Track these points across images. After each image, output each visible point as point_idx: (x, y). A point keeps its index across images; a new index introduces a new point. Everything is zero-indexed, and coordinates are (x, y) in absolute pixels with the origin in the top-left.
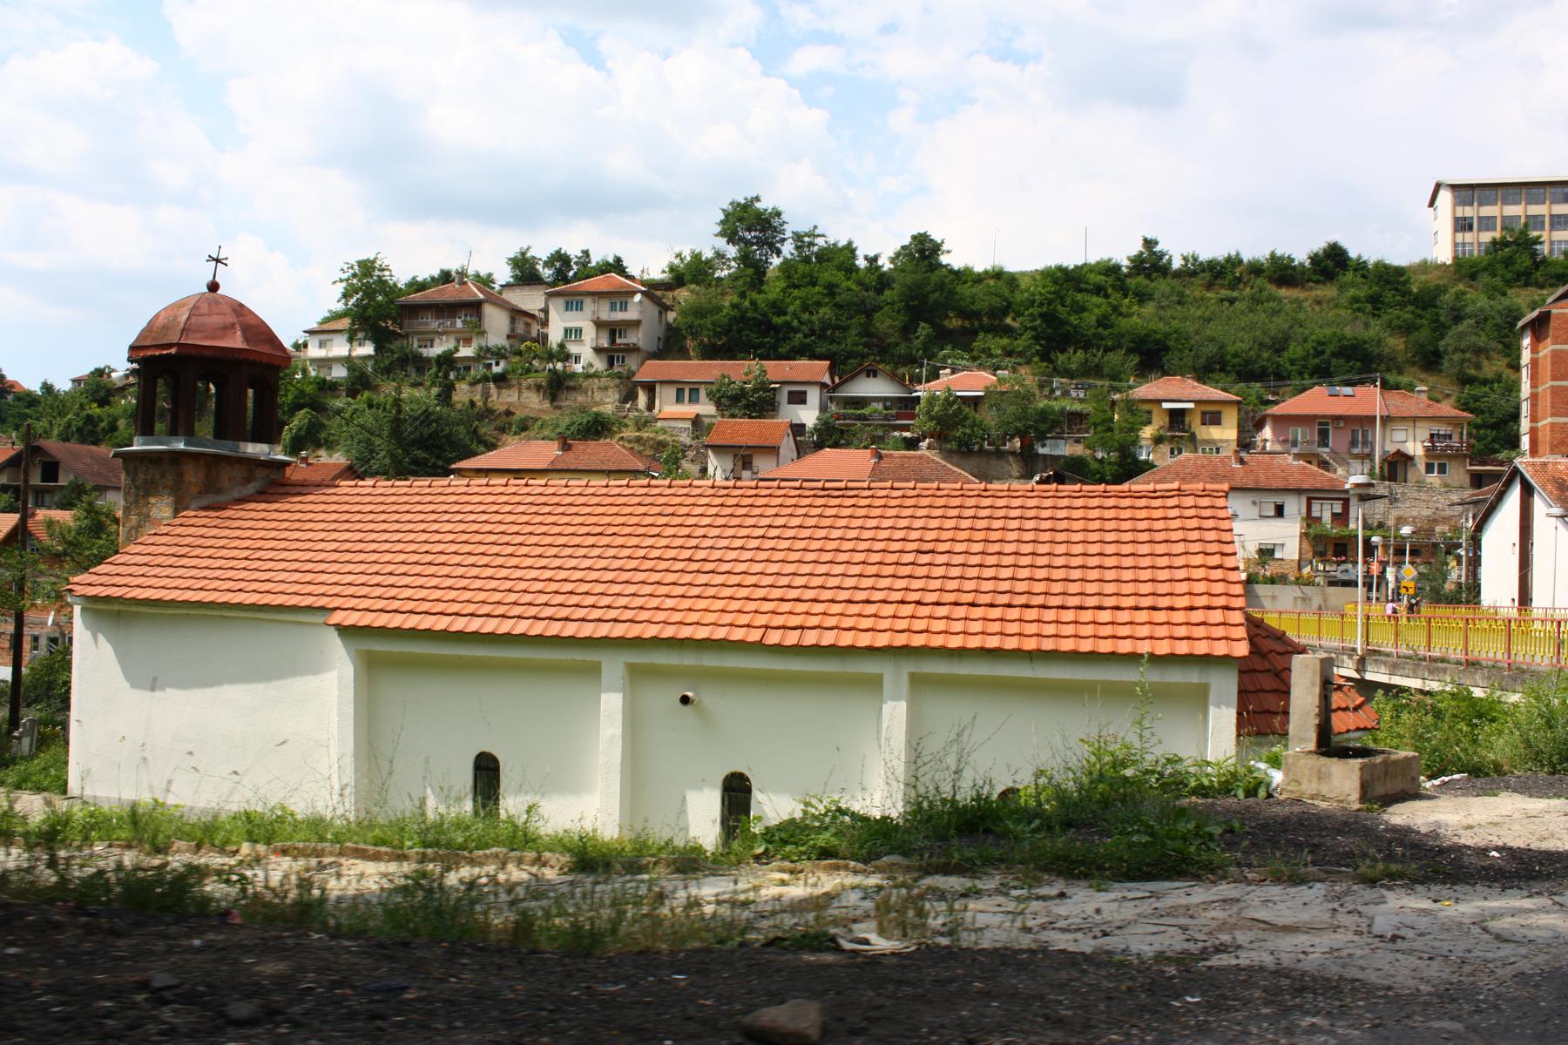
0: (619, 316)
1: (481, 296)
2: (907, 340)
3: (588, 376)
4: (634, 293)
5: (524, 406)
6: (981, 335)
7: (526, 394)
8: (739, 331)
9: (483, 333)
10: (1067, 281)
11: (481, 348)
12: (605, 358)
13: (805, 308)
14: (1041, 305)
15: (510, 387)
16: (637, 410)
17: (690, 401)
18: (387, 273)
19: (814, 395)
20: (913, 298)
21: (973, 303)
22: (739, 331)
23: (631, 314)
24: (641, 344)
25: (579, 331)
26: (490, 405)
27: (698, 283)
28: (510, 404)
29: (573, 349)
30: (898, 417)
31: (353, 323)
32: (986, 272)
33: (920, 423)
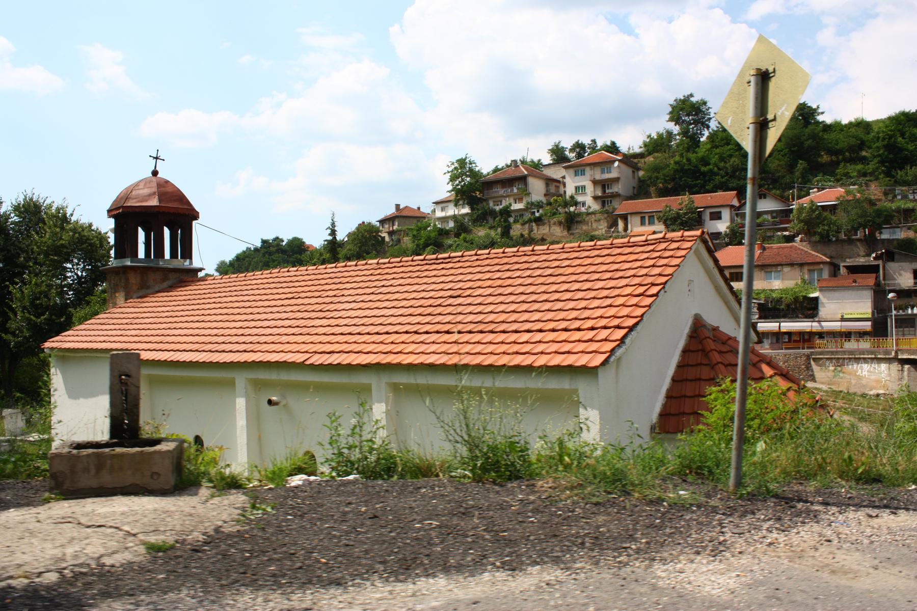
0: (607, 176)
1: (526, 173)
2: (792, 173)
3: (588, 214)
4: (614, 161)
5: (552, 235)
6: (842, 164)
7: (553, 228)
8: (680, 178)
9: (529, 194)
10: (909, 121)
11: (528, 203)
12: (600, 202)
13: (722, 159)
14: (884, 139)
15: (544, 224)
16: (618, 232)
17: (649, 224)
18: (474, 165)
19: (726, 214)
20: (794, 146)
21: (837, 144)
22: (680, 178)
23: (614, 174)
24: (621, 192)
25: (584, 187)
26: (532, 235)
27: (657, 152)
28: (544, 234)
29: (580, 199)
30: (782, 222)
31: (457, 196)
32: (851, 123)
33: (794, 225)
